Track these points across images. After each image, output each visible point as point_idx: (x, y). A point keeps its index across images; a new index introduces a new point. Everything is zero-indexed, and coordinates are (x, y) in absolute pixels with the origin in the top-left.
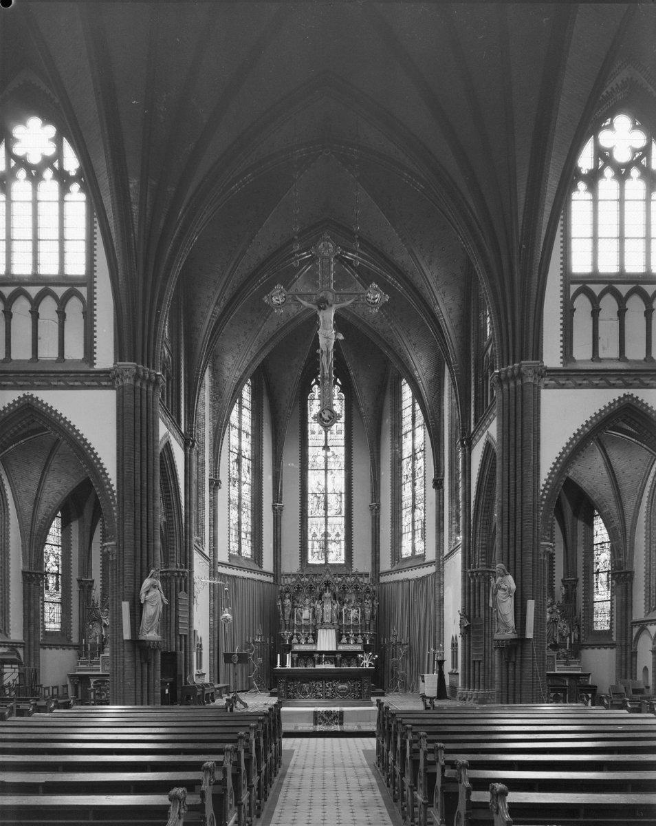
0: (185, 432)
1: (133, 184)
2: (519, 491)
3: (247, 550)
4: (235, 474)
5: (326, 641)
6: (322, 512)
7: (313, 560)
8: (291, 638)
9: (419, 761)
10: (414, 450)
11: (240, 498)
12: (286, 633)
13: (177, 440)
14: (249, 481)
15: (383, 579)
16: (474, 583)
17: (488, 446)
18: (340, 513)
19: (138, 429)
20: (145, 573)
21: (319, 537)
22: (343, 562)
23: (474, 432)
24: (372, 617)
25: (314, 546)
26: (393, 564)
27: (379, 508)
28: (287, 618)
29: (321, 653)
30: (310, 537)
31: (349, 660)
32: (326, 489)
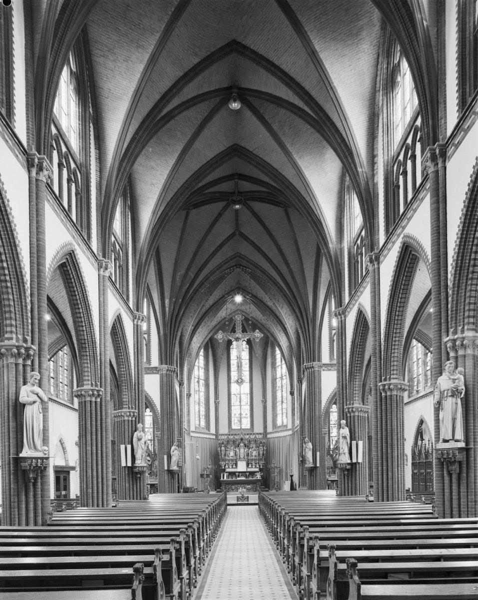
0: (28, 145)
1: (167, 301)
2: (313, 411)
3: (203, 424)
4: (197, 388)
5: (242, 467)
6: (239, 403)
7: (235, 426)
8: (225, 466)
9: (304, 545)
10: (282, 375)
11: (199, 399)
12: (222, 463)
13: (84, 252)
14: (203, 390)
15: (269, 436)
16: (386, 397)
17: (361, 314)
18: (247, 404)
19: (168, 390)
20: (171, 445)
21: (237, 416)
22: (249, 428)
23: (365, 275)
24: (263, 455)
25: (235, 420)
26: (273, 429)
28: (223, 456)
29: (239, 472)
30: (233, 415)
31: (232, 476)
32: (240, 392)
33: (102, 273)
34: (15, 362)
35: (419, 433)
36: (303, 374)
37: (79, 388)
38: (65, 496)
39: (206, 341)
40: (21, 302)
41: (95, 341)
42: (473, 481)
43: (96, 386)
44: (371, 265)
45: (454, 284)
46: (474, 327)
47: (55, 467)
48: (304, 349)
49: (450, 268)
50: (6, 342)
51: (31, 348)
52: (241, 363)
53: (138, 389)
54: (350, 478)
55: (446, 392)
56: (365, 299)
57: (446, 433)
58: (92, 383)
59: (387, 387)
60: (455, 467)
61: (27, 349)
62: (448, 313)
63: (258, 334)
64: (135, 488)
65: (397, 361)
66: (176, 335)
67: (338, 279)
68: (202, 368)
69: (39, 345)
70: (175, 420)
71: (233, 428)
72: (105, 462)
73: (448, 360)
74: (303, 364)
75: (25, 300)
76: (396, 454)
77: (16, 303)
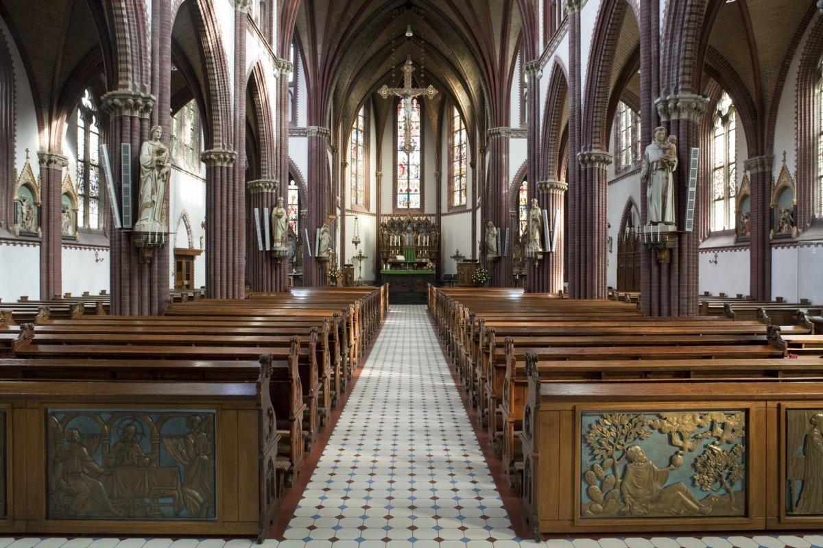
1: (319, 47)
7: (400, 206)
16: (586, 170)
17: (557, 68)
21: (404, 192)
23: (564, 21)
26: (449, 209)
27: (440, 175)
33: (239, 9)
34: (130, 115)
35: (627, 217)
36: (487, 141)
37: (207, 151)
38: (188, 287)
39: (367, 97)
40: (140, 42)
41: (229, 92)
42: (686, 273)
43: (229, 147)
44: (571, 8)
45: (666, 34)
46: (690, 86)
47: (176, 250)
48: (488, 110)
49: (662, 15)
50: (121, 91)
51: (150, 98)
52: (410, 125)
53: (281, 154)
54: (541, 271)
55: (655, 164)
56: (562, 51)
57: (654, 212)
58: (223, 144)
59: (587, 158)
60: (665, 256)
61: (146, 99)
62: (659, 69)
63: (431, 91)
64: (274, 278)
65: (600, 126)
66: (330, 89)
67: (531, 26)
68: (361, 131)
69: (160, 95)
70: (326, 195)
71: (398, 207)
72: (237, 243)
73: (659, 125)
74: (487, 128)
75: (145, 39)
76: (597, 241)
77: (134, 43)
